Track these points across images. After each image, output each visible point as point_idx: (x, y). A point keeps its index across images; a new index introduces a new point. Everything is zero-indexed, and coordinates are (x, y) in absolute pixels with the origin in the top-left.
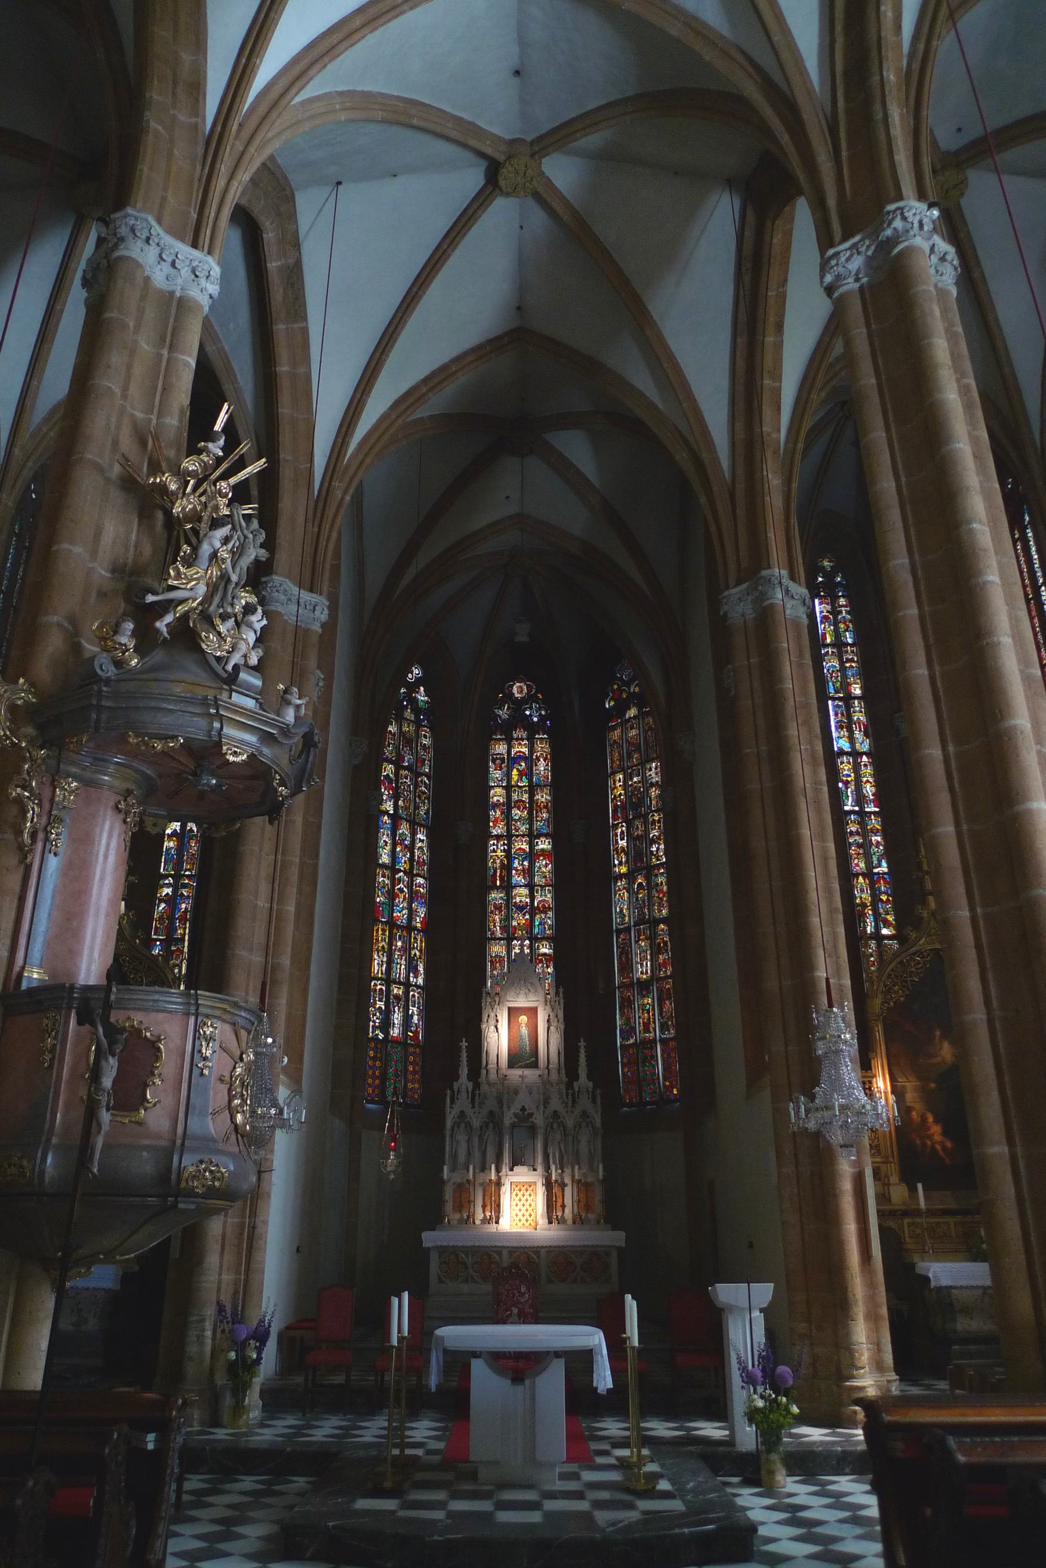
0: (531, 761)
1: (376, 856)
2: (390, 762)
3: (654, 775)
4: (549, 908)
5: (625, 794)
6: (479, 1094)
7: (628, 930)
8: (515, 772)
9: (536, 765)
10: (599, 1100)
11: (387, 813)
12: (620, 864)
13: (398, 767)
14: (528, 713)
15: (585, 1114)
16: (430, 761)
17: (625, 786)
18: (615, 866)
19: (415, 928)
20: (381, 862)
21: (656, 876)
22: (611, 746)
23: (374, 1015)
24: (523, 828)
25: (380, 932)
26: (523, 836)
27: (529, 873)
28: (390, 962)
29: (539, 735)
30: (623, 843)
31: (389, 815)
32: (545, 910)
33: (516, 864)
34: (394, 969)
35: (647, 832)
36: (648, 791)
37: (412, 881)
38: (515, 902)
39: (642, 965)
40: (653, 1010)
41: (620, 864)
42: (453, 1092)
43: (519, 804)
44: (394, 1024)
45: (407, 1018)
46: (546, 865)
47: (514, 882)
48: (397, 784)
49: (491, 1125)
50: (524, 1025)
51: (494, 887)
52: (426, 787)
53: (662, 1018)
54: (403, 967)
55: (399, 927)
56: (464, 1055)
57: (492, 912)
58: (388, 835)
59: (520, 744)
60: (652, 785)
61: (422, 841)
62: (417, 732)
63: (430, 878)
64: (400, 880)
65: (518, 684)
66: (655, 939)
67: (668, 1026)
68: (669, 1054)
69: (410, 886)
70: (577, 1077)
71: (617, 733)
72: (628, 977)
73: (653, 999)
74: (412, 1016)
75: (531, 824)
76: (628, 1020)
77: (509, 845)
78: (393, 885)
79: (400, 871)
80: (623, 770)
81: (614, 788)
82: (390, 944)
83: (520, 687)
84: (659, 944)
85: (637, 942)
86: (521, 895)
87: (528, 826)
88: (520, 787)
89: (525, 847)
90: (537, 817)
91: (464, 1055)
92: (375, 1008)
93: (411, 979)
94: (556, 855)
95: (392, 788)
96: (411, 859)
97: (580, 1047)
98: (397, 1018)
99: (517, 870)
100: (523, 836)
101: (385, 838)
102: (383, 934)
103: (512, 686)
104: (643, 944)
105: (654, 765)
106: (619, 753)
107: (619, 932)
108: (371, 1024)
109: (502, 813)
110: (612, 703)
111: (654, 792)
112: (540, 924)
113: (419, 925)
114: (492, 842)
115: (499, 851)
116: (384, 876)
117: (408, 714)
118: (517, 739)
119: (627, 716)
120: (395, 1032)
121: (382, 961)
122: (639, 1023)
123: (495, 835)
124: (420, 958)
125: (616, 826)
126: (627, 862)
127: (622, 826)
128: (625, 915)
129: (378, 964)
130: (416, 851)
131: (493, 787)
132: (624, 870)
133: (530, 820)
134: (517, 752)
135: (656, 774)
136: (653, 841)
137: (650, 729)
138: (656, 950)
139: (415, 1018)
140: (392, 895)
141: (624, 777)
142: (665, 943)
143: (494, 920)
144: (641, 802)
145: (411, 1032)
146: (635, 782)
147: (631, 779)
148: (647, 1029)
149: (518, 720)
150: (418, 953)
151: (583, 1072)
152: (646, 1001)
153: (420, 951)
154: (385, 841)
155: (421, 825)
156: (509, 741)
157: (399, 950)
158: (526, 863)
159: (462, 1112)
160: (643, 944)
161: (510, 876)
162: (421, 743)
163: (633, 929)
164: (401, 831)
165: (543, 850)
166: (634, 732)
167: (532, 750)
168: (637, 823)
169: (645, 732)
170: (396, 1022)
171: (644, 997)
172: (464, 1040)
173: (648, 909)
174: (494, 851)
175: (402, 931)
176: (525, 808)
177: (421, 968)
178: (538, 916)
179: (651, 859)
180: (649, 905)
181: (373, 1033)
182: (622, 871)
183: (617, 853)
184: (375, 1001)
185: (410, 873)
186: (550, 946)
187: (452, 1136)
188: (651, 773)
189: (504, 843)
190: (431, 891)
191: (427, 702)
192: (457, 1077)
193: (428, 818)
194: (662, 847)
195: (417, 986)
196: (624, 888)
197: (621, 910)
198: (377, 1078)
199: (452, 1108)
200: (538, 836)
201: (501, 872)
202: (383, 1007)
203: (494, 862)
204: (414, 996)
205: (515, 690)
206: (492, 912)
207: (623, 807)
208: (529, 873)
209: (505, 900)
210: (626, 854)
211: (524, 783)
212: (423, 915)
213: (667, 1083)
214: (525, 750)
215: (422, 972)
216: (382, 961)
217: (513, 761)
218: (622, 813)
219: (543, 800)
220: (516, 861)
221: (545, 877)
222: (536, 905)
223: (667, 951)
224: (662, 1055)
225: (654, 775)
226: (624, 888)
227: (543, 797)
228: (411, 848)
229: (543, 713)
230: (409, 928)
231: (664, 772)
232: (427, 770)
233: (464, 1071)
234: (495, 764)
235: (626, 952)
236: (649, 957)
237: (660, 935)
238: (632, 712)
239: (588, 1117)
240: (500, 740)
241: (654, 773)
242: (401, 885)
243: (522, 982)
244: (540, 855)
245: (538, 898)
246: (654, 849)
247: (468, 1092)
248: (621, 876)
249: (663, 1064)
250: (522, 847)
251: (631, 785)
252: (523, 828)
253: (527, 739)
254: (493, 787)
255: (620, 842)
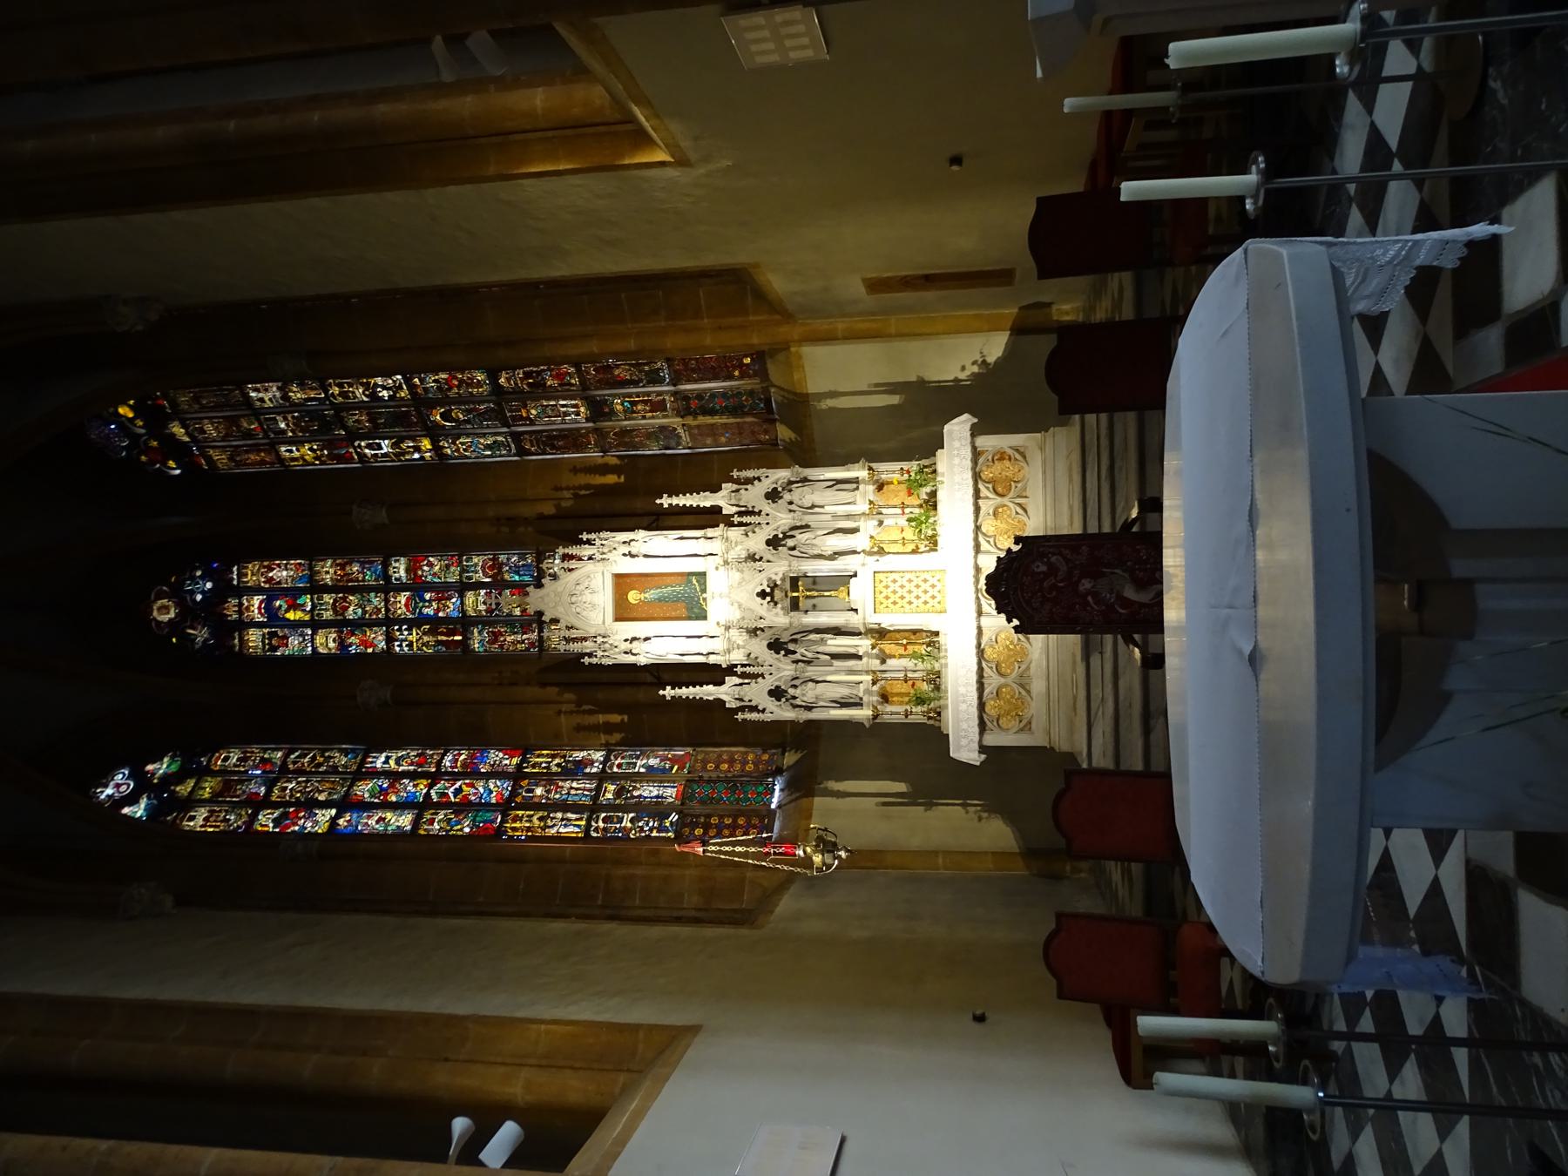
0: (273, 592)
1: (400, 834)
2: (253, 818)
3: (270, 395)
4: (495, 559)
5: (309, 442)
6: (743, 666)
7: (516, 437)
8: (291, 616)
9: (279, 583)
10: (750, 474)
11: (333, 820)
12: (417, 449)
13: (266, 803)
14: (199, 597)
15: (773, 496)
16: (265, 750)
17: (298, 442)
18: (422, 458)
19: (519, 767)
20: (409, 828)
21: (426, 390)
22: (239, 464)
23: (641, 828)
24: (376, 600)
25: (517, 825)
26: (387, 601)
27: (443, 591)
28: (564, 807)
29: (233, 579)
30: (386, 446)
31: (338, 816)
32: (497, 566)
33: (429, 611)
34: (576, 798)
35: (360, 406)
36: (296, 405)
37: (447, 773)
38: (486, 611)
39: (566, 414)
40: (630, 395)
41: (417, 449)
42: (742, 709)
43: (340, 609)
44: (657, 797)
45: (652, 775)
46: (431, 565)
47: (455, 614)
48: (289, 804)
49: (791, 647)
50: (642, 596)
51: (465, 644)
52: (305, 756)
53: (640, 380)
54: (575, 785)
55: (514, 793)
56: (684, 692)
57: (501, 647)
58: (369, 817)
59: (248, 609)
60: (285, 397)
61: (388, 758)
62: (214, 774)
63: (445, 743)
64: (443, 795)
65: (155, 613)
66: (522, 392)
67: (651, 371)
68: (693, 370)
69: (455, 777)
70: (716, 510)
71: (216, 455)
72: (586, 436)
73: (615, 396)
74: (650, 768)
75: (370, 589)
76: (649, 436)
77: (400, 622)
78: (448, 805)
79: (428, 795)
80: (272, 447)
81: (305, 460)
82: (537, 807)
83: (159, 609)
84: (529, 385)
85: (532, 423)
86: (475, 602)
87: (372, 595)
88: (314, 607)
89: (403, 598)
90: (358, 581)
91: (684, 692)
92: (631, 829)
93: (594, 770)
94: (416, 551)
95: (297, 812)
96: (413, 776)
97: (670, 505)
98: (649, 791)
99: (438, 610)
100: (387, 601)
101: (372, 822)
102: (521, 819)
103: (159, 623)
104: (533, 412)
105: (253, 394)
106: (247, 452)
107: (522, 452)
108: (654, 834)
109: (353, 634)
110: (172, 464)
111: (297, 395)
112: (517, 573)
113: (515, 761)
114: (397, 649)
115: (410, 638)
116: (432, 822)
117: (184, 789)
118: (240, 612)
119: (186, 439)
120: (670, 793)
121: (562, 820)
122: (653, 417)
123: (387, 644)
124: (564, 757)
125: (362, 456)
126: (413, 439)
127: (359, 446)
128: (495, 442)
129: (565, 826)
130: (401, 769)
131: (314, 649)
132: (426, 444)
133: (363, 590)
134: (260, 612)
135: (266, 390)
136: (374, 396)
137: (196, 399)
138: (539, 390)
139: (653, 762)
140: (464, 807)
141: (284, 443)
142: (527, 375)
143: (514, 643)
144: (315, 415)
145: (672, 768)
146: (287, 425)
147: (283, 432)
148: (658, 407)
149: (211, 611)
150: (557, 761)
151: (704, 500)
152: (619, 407)
153: (553, 757)
154: (377, 822)
155: (363, 761)
156: (244, 625)
157: (548, 792)
158: (427, 596)
159: (772, 693)
160: (533, 412)
161: (448, 620)
162: (235, 766)
163: (514, 429)
164: (367, 795)
165: (407, 571)
166: (209, 428)
167: (258, 590)
168: (350, 423)
169: (203, 408)
170: (655, 793)
171: (612, 413)
172: (661, 692)
173: (480, 403)
174: (410, 645)
175: (522, 787)
176: (344, 599)
177: (579, 755)
178: (507, 577)
179: (402, 399)
180: (474, 403)
181: (668, 831)
182: (429, 447)
183: (403, 454)
184: (620, 830)
185: (434, 778)
186: (549, 557)
187: (809, 708)
188: (266, 399)
189: (399, 630)
190: (463, 742)
191: (172, 758)
192: (720, 703)
193: (353, 751)
194: (379, 380)
195: (607, 759)
196: (454, 443)
197: (488, 447)
198: (735, 821)
199: (763, 711)
200: (387, 578)
201: (442, 634)
202: (631, 815)
203: (426, 644)
204: (619, 766)
205: (165, 618)
206: (501, 647)
207: (329, 444)
208: (443, 591)
209: (484, 626)
210: (402, 440)
211: (307, 600)
212: (501, 755)
213: (737, 373)
214: (256, 600)
215: (585, 753)
216: (562, 820)
217: (273, 617)
218: (341, 448)
219: (332, 571)
220: (426, 611)
221: (448, 567)
222: (488, 580)
223: (539, 373)
224: (696, 381)
225: (270, 395)
226: (454, 443)
227: (328, 571)
228: (395, 777)
229: (199, 573)
230: (517, 776)
231: (263, 378)
232: (280, 754)
233: (708, 692)
234: (278, 647)
235: (551, 440)
236: (552, 403)
237: (516, 384)
238: (178, 430)
239: (775, 489)
240: (241, 639)
241: (266, 395)
242: (450, 792)
243: (574, 599)
244: (415, 574)
245: (480, 577)
246: (385, 394)
247: (741, 684)
248: (437, 448)
249: (710, 380)
250: (403, 602)
251: (292, 431)
252: (376, 601)
253: (240, 597)
254: (314, 649)
255: (385, 450)
